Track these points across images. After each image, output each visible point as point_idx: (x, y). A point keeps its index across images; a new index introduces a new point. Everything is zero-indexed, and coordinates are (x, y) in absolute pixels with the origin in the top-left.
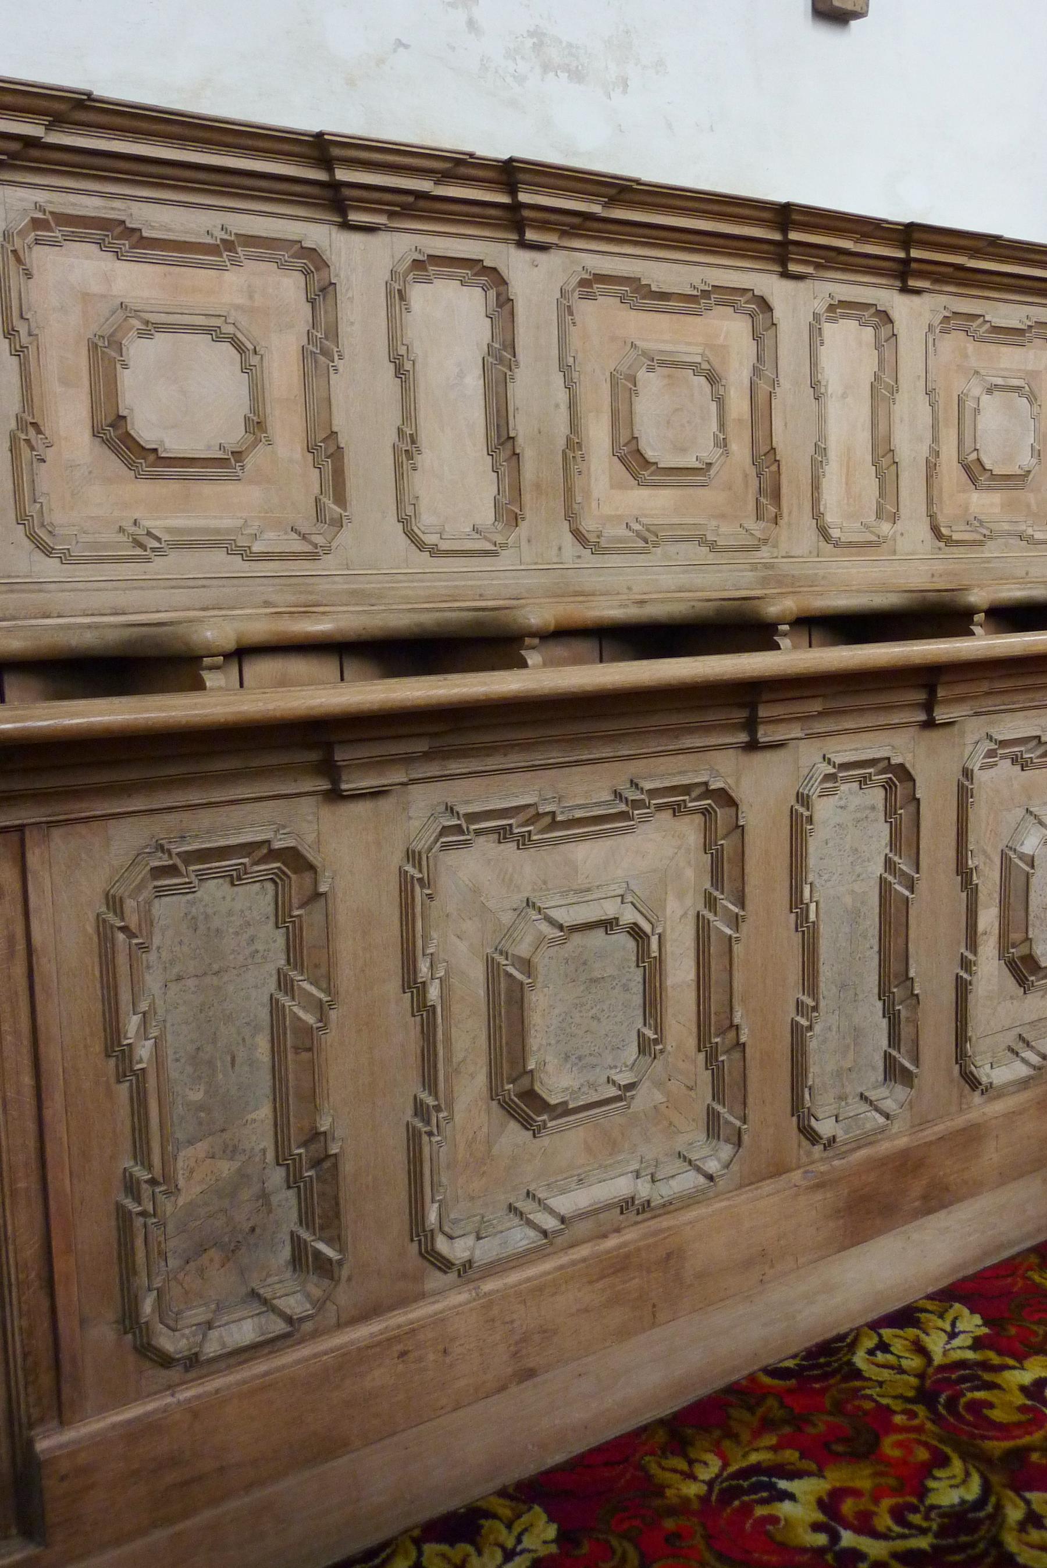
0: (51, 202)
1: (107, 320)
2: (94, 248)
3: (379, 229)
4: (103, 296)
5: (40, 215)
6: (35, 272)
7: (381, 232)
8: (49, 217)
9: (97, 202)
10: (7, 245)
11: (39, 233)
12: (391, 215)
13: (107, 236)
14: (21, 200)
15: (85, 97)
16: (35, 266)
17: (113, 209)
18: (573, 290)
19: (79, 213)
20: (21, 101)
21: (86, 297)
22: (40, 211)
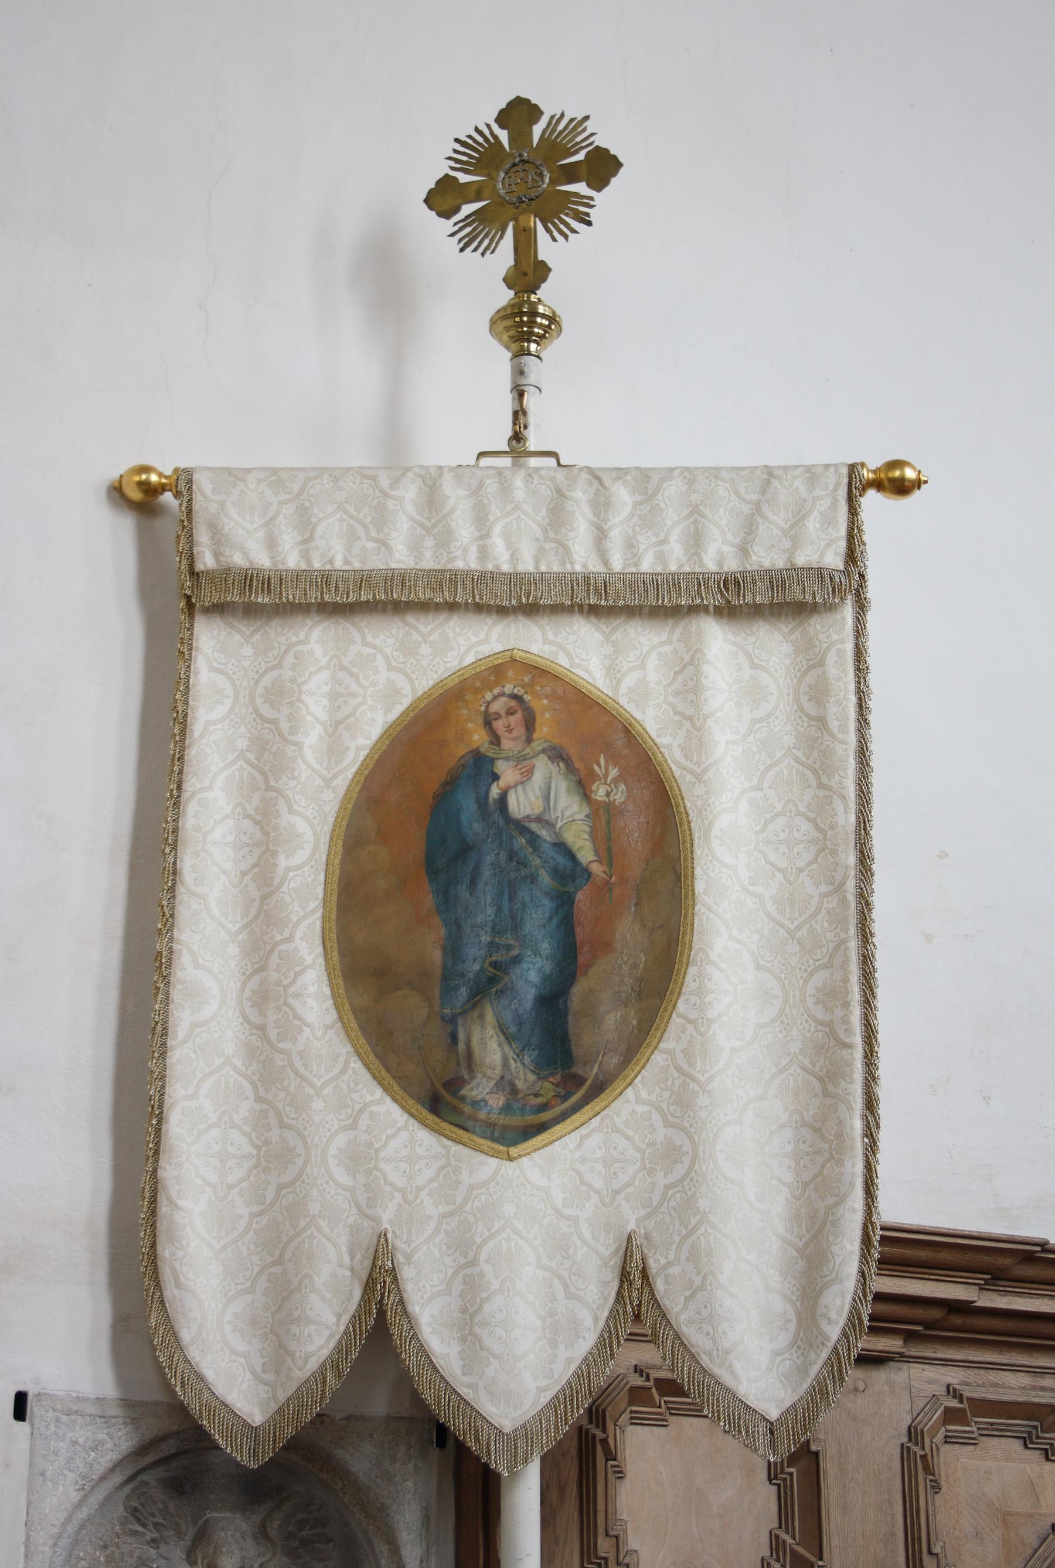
0: (968, 1384)
1: (1036, 1551)
2: (1016, 1445)
3: (892, 1359)
4: (1030, 1516)
5: (954, 1404)
6: (943, 1484)
7: (892, 1364)
8: (965, 1405)
9: (1024, 1380)
10: (915, 1448)
11: (950, 1427)
12: (910, 1337)
13: (1035, 1427)
14: (931, 1382)
15: (1039, 1249)
16: (943, 1474)
17: (1043, 1389)
18: (934, 1431)
19: (1005, 1398)
20: (959, 1258)
21: (1006, 1518)
22: (954, 1397)
